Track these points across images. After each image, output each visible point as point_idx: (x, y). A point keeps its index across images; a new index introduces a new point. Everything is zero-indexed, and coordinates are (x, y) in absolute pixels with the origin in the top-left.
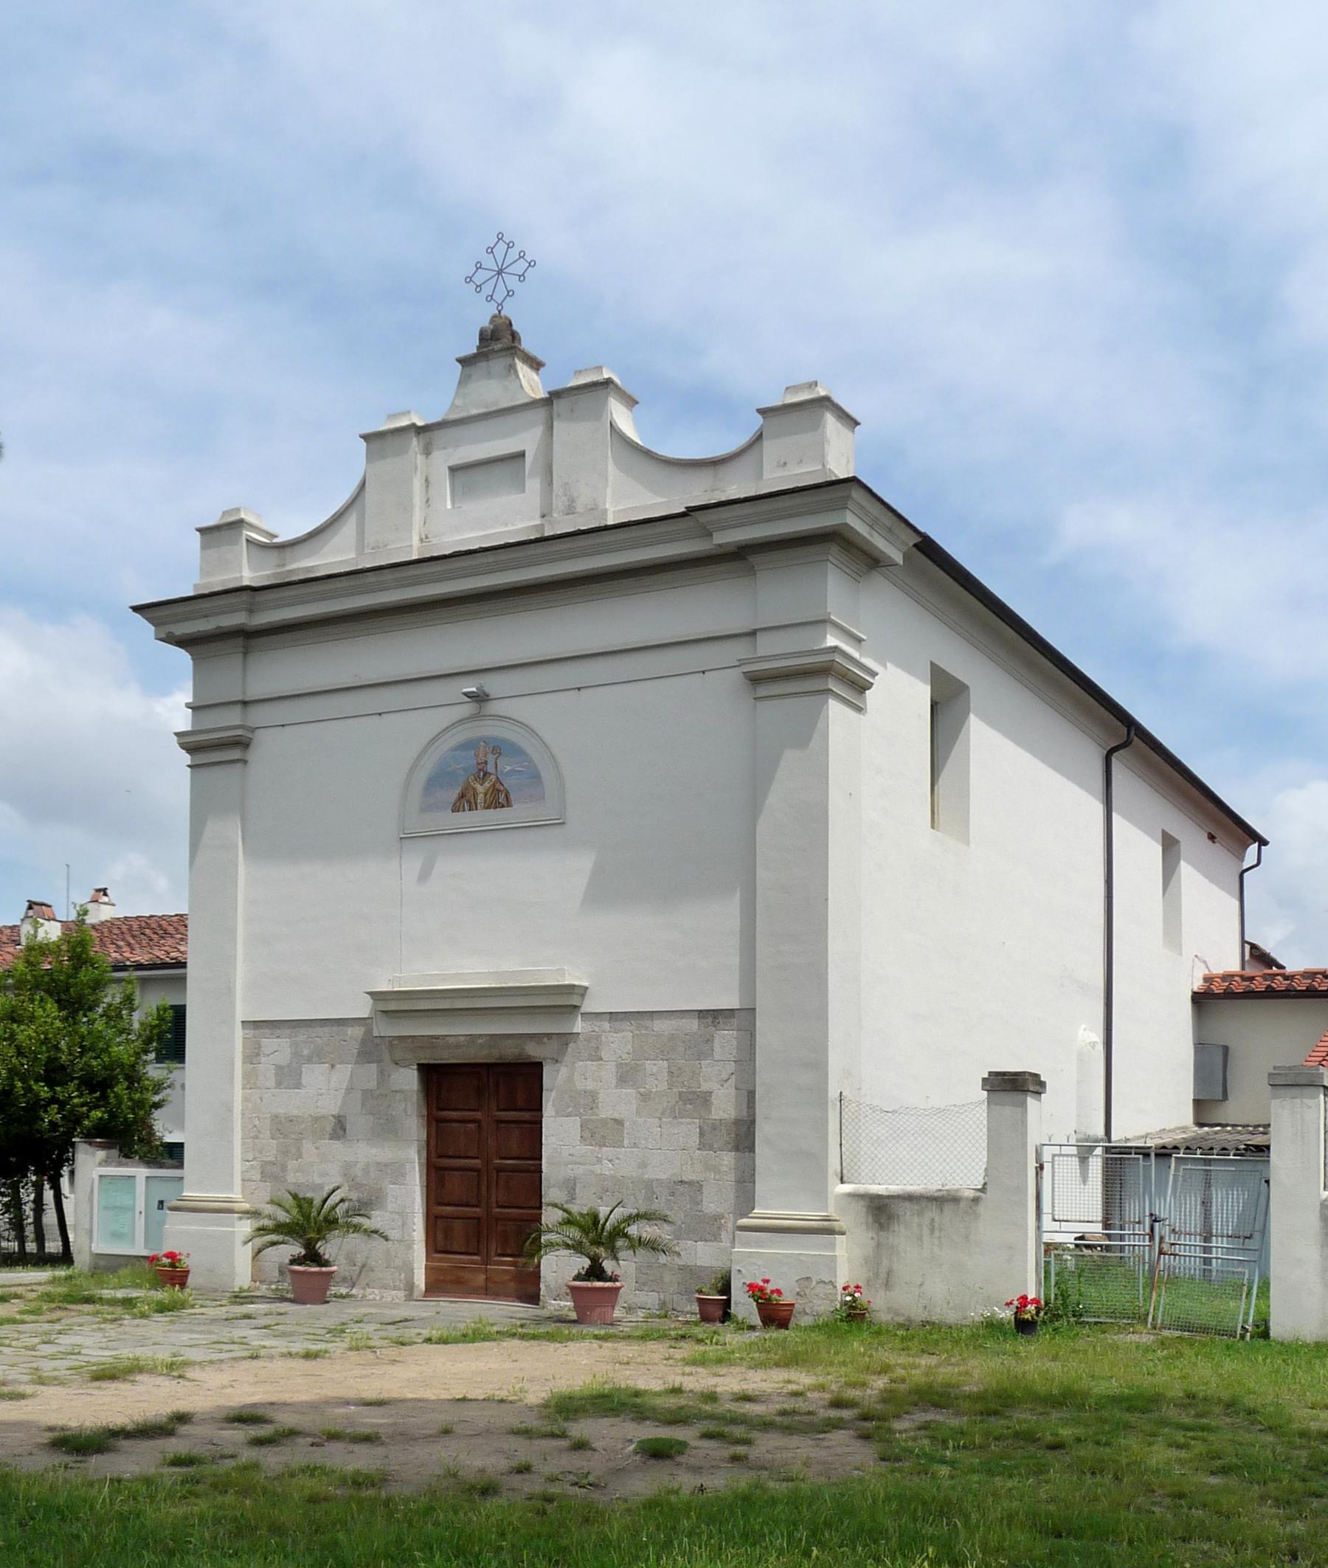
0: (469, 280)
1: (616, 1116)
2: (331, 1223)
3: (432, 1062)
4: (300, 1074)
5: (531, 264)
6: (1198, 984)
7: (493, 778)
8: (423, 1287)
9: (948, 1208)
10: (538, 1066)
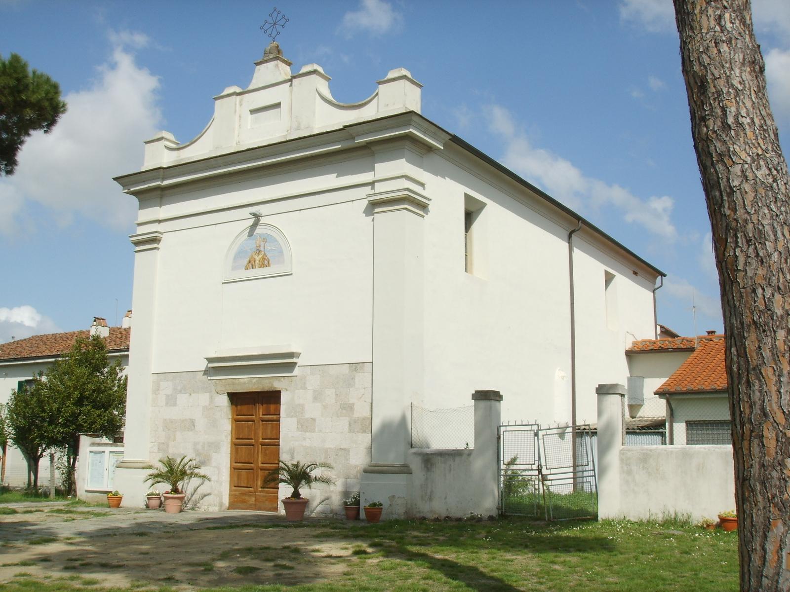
0: (287, 20)
1: (312, 416)
2: (183, 473)
3: (233, 392)
4: (176, 398)
5: (262, 28)
6: (629, 346)
7: (263, 253)
8: (227, 505)
9: (457, 459)
10: (279, 392)
